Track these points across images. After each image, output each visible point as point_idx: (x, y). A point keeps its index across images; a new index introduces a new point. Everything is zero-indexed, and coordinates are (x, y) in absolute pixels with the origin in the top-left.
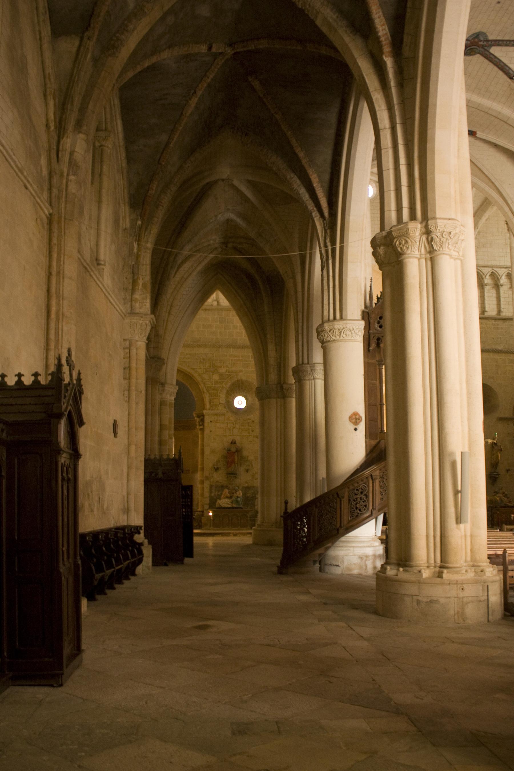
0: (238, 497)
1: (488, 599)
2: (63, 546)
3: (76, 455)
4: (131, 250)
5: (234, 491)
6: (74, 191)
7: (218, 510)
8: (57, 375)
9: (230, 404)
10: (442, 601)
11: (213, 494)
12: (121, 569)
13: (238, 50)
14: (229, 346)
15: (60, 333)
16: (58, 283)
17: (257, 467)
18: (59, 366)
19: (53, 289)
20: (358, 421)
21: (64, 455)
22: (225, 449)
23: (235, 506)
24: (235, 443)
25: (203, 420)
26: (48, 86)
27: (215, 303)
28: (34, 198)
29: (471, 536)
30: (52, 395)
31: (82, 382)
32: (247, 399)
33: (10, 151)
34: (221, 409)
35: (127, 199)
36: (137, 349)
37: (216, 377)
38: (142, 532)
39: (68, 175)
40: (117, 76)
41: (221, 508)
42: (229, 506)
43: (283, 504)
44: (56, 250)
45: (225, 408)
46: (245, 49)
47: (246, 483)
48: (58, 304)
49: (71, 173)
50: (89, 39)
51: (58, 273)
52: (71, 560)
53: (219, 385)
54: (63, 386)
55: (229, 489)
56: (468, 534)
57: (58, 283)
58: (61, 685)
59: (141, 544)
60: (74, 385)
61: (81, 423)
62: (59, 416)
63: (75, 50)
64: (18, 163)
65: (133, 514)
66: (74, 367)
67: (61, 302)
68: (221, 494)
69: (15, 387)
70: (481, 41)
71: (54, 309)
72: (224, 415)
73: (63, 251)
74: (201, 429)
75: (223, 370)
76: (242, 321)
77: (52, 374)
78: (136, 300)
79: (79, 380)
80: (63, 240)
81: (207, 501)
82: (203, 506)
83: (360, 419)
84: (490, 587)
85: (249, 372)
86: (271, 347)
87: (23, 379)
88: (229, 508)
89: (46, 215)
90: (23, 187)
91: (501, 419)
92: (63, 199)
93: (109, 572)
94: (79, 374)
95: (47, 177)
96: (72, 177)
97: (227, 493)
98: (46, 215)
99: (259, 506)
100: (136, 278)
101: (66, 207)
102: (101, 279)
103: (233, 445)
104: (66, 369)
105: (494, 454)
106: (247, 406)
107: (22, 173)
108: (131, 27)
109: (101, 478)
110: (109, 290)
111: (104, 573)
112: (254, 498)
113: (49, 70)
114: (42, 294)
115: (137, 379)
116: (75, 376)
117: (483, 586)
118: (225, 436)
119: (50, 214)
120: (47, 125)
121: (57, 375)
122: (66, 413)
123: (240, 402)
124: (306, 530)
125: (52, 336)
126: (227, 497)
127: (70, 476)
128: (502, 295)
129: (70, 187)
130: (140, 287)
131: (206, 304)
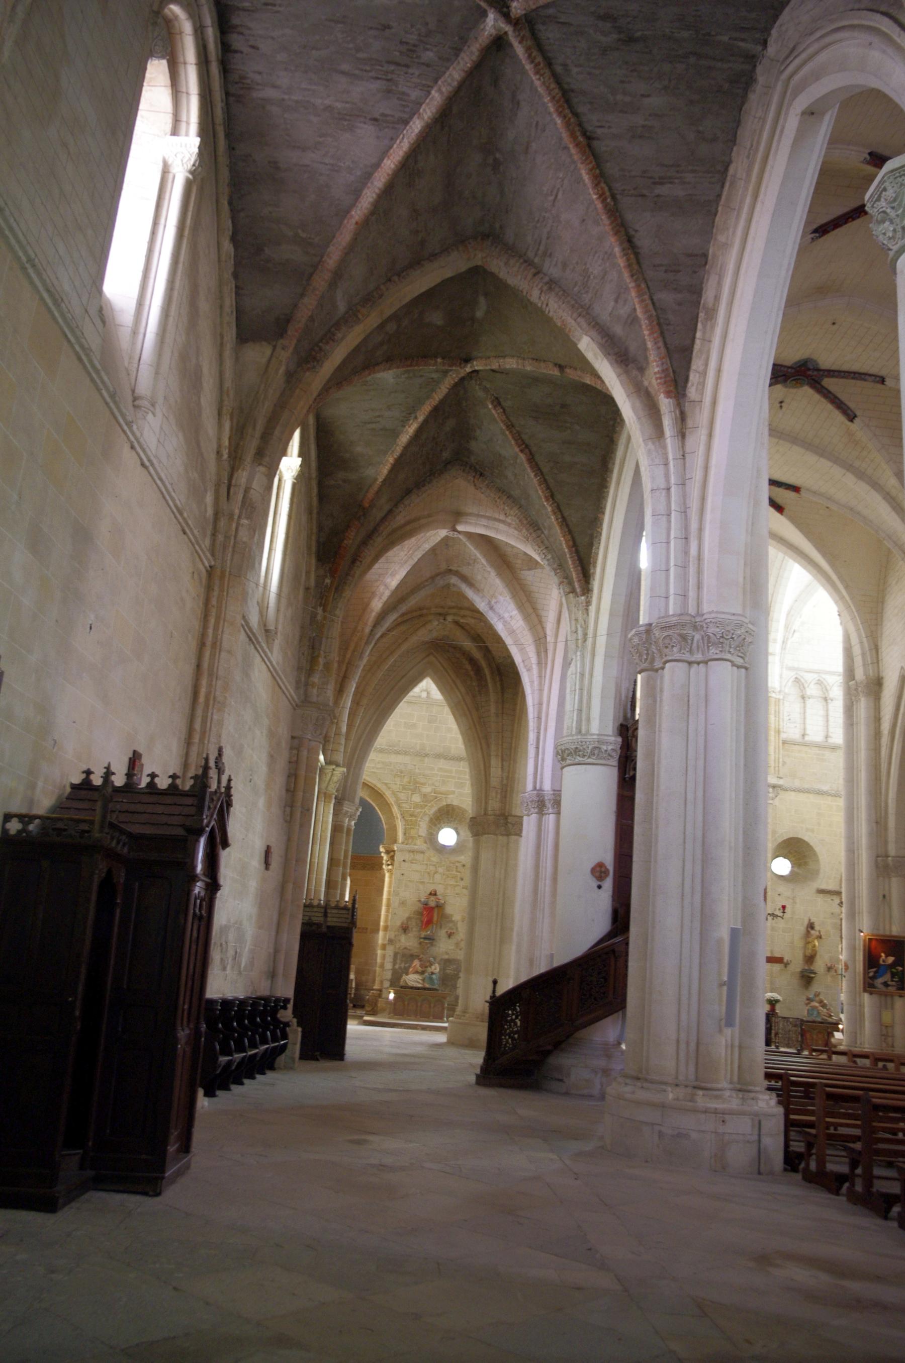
0: (432, 973)
1: (759, 1141)
2: (184, 1003)
3: (213, 886)
4: (313, 616)
5: (428, 964)
6: (245, 539)
7: (403, 991)
8: (202, 780)
9: (432, 839)
10: (694, 1135)
11: (397, 967)
12: (255, 1054)
13: (476, 368)
14: (438, 756)
15: (208, 724)
16: (212, 656)
17: (462, 932)
18: (206, 768)
19: (205, 665)
20: (603, 875)
21: (198, 884)
22: (420, 901)
23: (427, 986)
24: (435, 894)
25: (392, 858)
26: (226, 403)
27: (424, 695)
28: (193, 545)
29: (740, 1047)
30: (192, 805)
31: (233, 791)
32: (458, 833)
33: (169, 486)
34: (420, 845)
35: (314, 549)
36: (309, 751)
37: (416, 798)
38: (290, 1006)
39: (239, 517)
40: (315, 395)
41: (406, 987)
42: (420, 986)
43: (491, 985)
44: (214, 614)
45: (426, 842)
46: (488, 368)
47: (447, 953)
48: (210, 685)
49: (244, 515)
50: (283, 349)
51: (214, 644)
52: (192, 1026)
53: (419, 810)
54: (208, 794)
55: (420, 960)
56: (737, 1043)
57: (212, 656)
58: (158, 1194)
59: (287, 1024)
60: (221, 793)
61: (225, 844)
62: (199, 832)
63: (264, 361)
64: (178, 502)
65: (280, 979)
66: (224, 771)
67: (214, 683)
68: (409, 967)
69: (146, 791)
70: (809, 370)
71: (203, 691)
72: (423, 852)
73: (223, 615)
74: (389, 871)
75: (427, 789)
76: (458, 723)
77: (195, 777)
78: (313, 685)
79: (228, 788)
80: (224, 602)
81: (388, 975)
82: (382, 982)
83: (606, 873)
84: (763, 1123)
85: (463, 795)
86: (495, 762)
87: (157, 780)
88: (418, 988)
89: (205, 567)
90: (181, 533)
91: (821, 892)
92: (231, 549)
93: (238, 1056)
94: (230, 780)
95: (211, 520)
96: (245, 521)
97: (418, 966)
98: (205, 567)
99: (460, 991)
100: (316, 654)
101: (232, 560)
102: (269, 654)
103: (432, 898)
104: (213, 773)
105: (809, 943)
106: (457, 844)
107: (181, 514)
108: (339, 335)
109: (241, 924)
110: (278, 668)
111: (230, 1058)
112: (457, 977)
113: (228, 384)
114: (189, 670)
115: (304, 792)
116: (224, 783)
117: (753, 1119)
118: (423, 883)
119: (211, 567)
120: (218, 453)
121: (202, 780)
122: (208, 829)
123: (448, 836)
124: (519, 1023)
125: (197, 726)
126: (417, 972)
127: (203, 912)
128: (831, 713)
129: (241, 533)
130: (321, 667)
131: (411, 694)
